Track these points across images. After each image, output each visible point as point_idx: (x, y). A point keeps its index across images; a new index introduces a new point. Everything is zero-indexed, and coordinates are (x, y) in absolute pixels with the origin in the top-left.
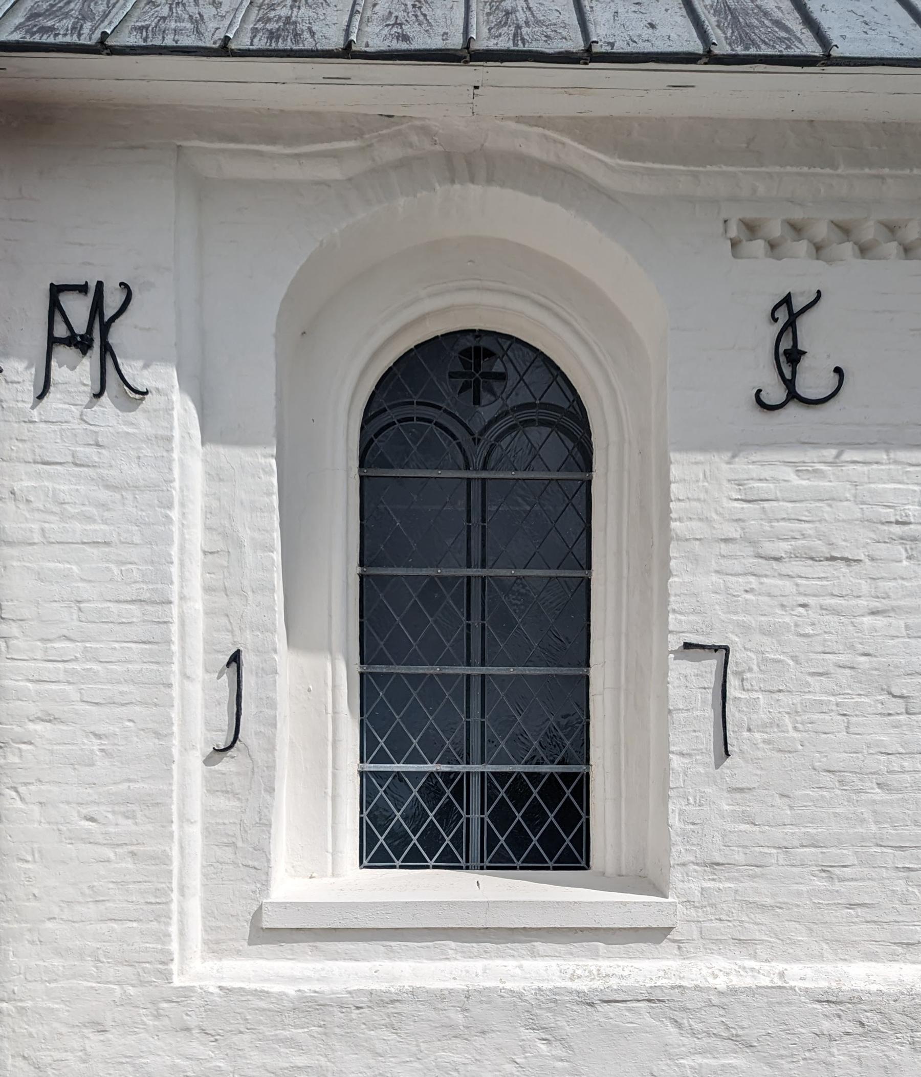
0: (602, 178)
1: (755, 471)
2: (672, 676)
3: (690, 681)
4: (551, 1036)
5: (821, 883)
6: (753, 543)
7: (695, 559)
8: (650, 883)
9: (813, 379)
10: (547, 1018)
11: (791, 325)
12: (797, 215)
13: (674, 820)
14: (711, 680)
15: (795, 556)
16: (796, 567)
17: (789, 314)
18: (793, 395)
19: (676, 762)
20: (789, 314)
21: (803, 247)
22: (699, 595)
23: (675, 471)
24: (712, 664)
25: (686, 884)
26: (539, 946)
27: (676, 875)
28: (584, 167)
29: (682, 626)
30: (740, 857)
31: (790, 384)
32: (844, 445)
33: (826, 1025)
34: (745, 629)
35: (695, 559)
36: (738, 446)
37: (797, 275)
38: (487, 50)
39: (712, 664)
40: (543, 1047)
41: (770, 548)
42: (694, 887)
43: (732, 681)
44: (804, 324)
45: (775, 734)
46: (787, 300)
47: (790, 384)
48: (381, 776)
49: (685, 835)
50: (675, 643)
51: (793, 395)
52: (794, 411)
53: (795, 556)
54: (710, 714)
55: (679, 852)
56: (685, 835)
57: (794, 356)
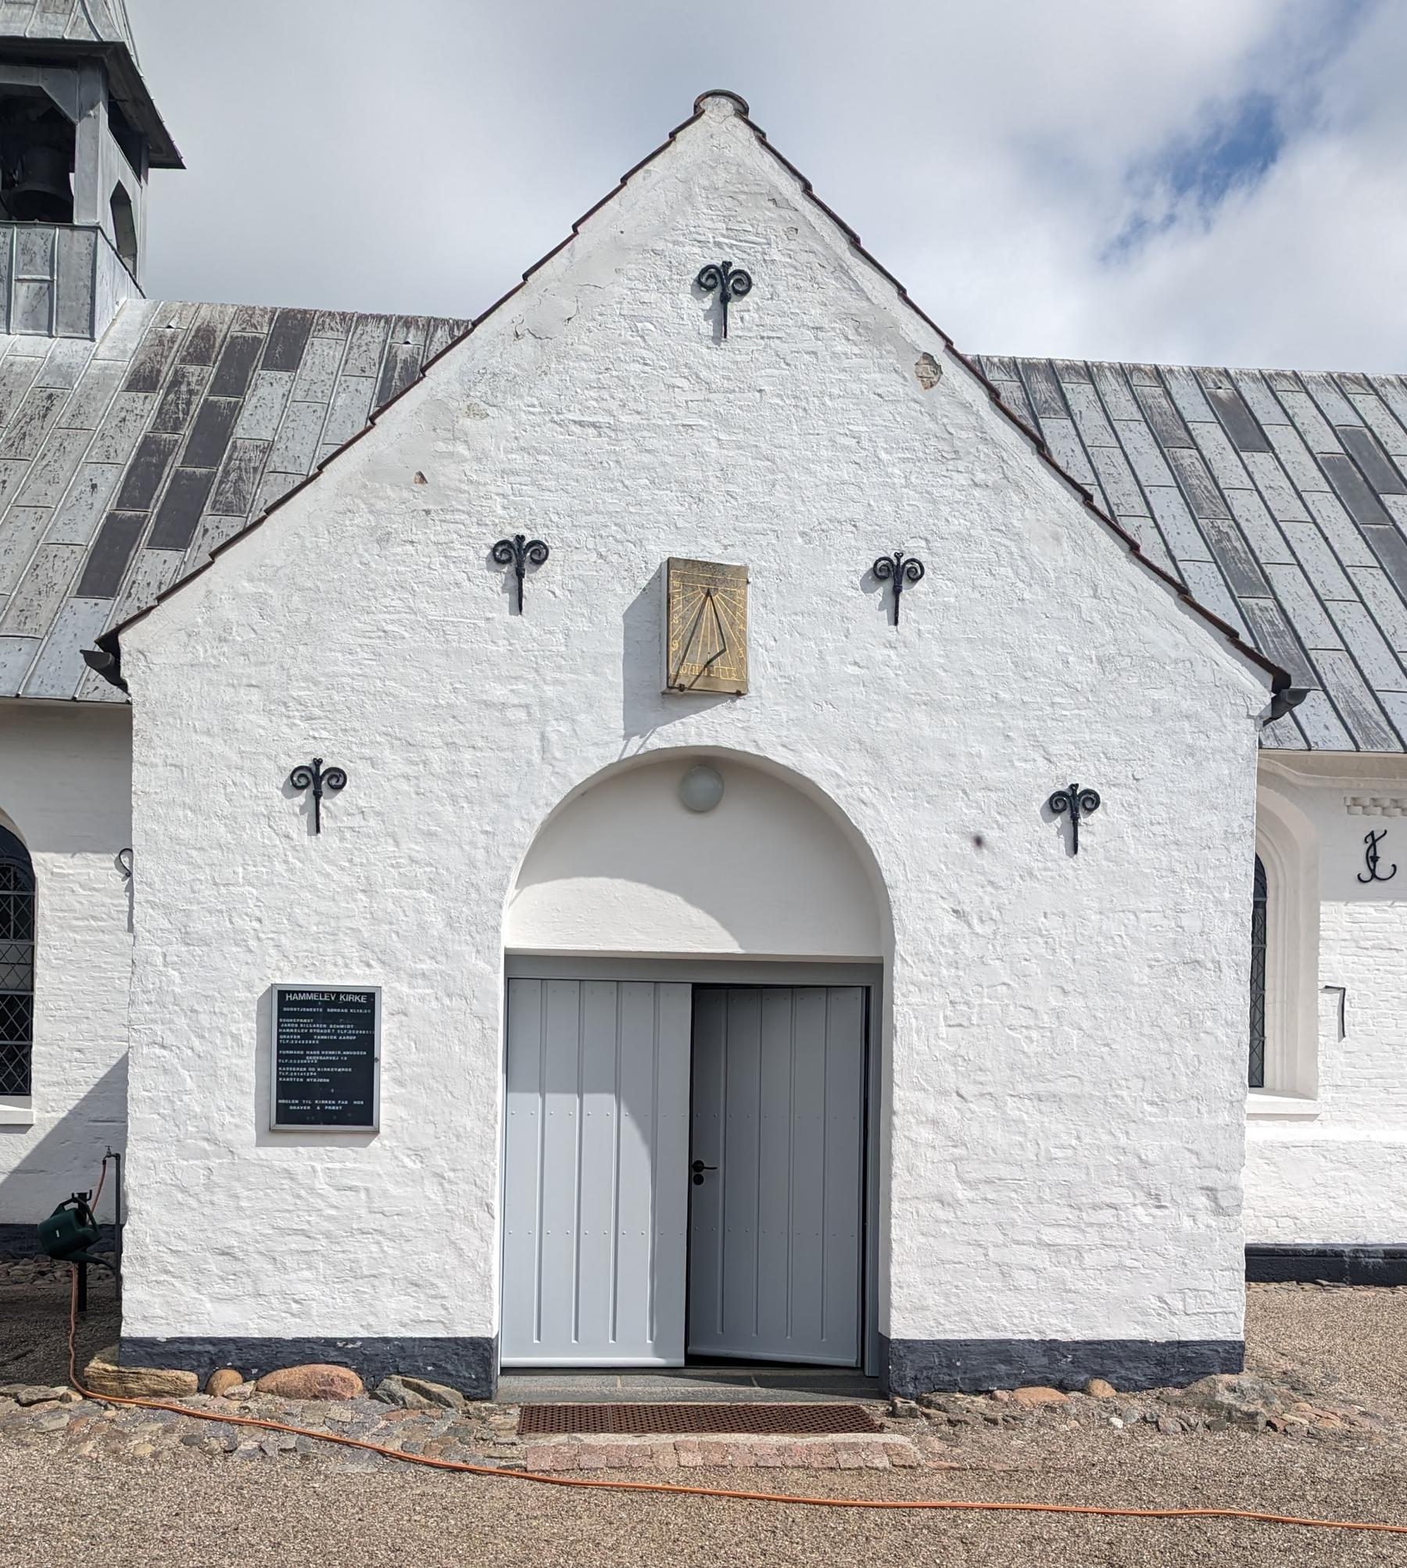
0: (1292, 779)
1: (1357, 909)
2: (1320, 1001)
3: (1328, 1004)
4: (1270, 1162)
5: (1383, 1095)
6: (1355, 941)
7: (1331, 949)
8: (1308, 1095)
9: (1382, 870)
10: (1268, 1154)
11: (1374, 844)
12: (1377, 796)
13: (1320, 1065)
14: (1337, 1003)
15: (1374, 947)
16: (1375, 952)
17: (1372, 840)
18: (1374, 876)
19: (1321, 1039)
20: (1372, 840)
21: (1379, 810)
22: (1333, 964)
23: (1322, 909)
24: (1338, 995)
25: (1325, 1094)
26: (1261, 1122)
27: (1321, 1090)
28: (1285, 775)
29: (1324, 978)
30: (1349, 1083)
31: (1373, 871)
32: (1395, 899)
33: (1389, 1158)
34: (1352, 980)
35: (1331, 949)
36: (1348, 899)
37: (1376, 823)
38: (884, 887)
39: (1338, 995)
40: (1266, 1167)
41: (1362, 944)
42: (1329, 1096)
43: (1346, 1004)
44: (1378, 844)
45: (1365, 1028)
46: (1372, 834)
47: (1373, 871)
48: (20, 1038)
49: (1324, 1072)
50: (1321, 986)
51: (1374, 876)
52: (1374, 881)
53: (1374, 947)
54: (1336, 1018)
55: (1322, 1080)
56: (1324, 1072)
57: (1375, 859)
